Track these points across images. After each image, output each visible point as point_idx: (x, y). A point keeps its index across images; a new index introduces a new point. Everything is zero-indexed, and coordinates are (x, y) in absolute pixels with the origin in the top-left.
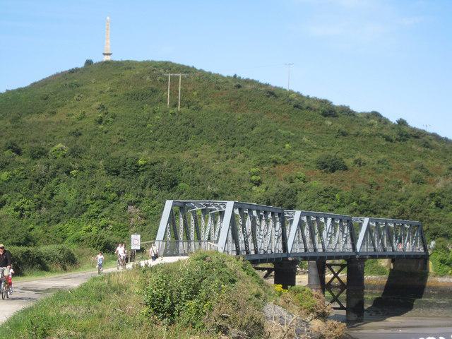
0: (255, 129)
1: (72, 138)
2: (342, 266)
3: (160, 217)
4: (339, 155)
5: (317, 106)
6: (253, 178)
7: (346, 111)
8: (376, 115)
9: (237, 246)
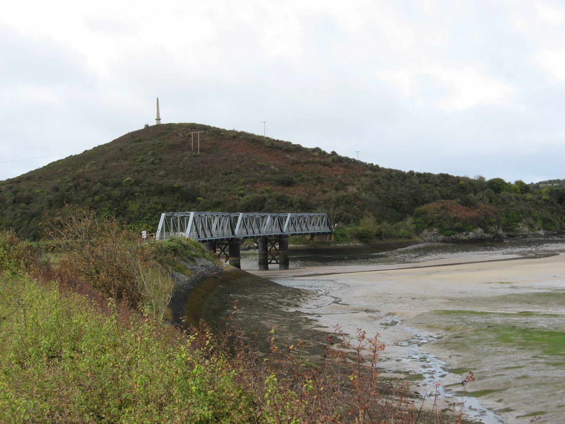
0: (244, 163)
1: (136, 174)
4: (291, 176)
6: (240, 192)
8: (317, 150)
9: (198, 234)
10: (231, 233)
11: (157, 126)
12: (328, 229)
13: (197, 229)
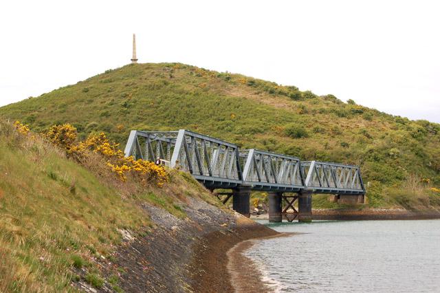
2: (295, 198)
3: (127, 138)
5: (286, 91)
7: (309, 95)
10: (237, 176)
11: (132, 65)
12: (359, 187)
13: (188, 158)
